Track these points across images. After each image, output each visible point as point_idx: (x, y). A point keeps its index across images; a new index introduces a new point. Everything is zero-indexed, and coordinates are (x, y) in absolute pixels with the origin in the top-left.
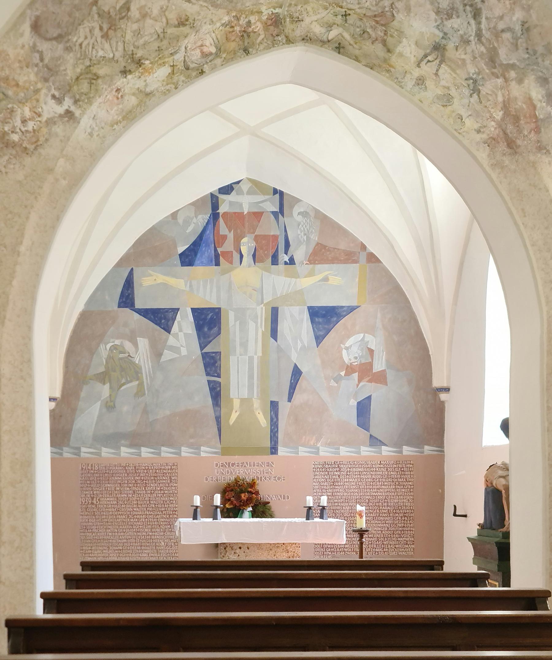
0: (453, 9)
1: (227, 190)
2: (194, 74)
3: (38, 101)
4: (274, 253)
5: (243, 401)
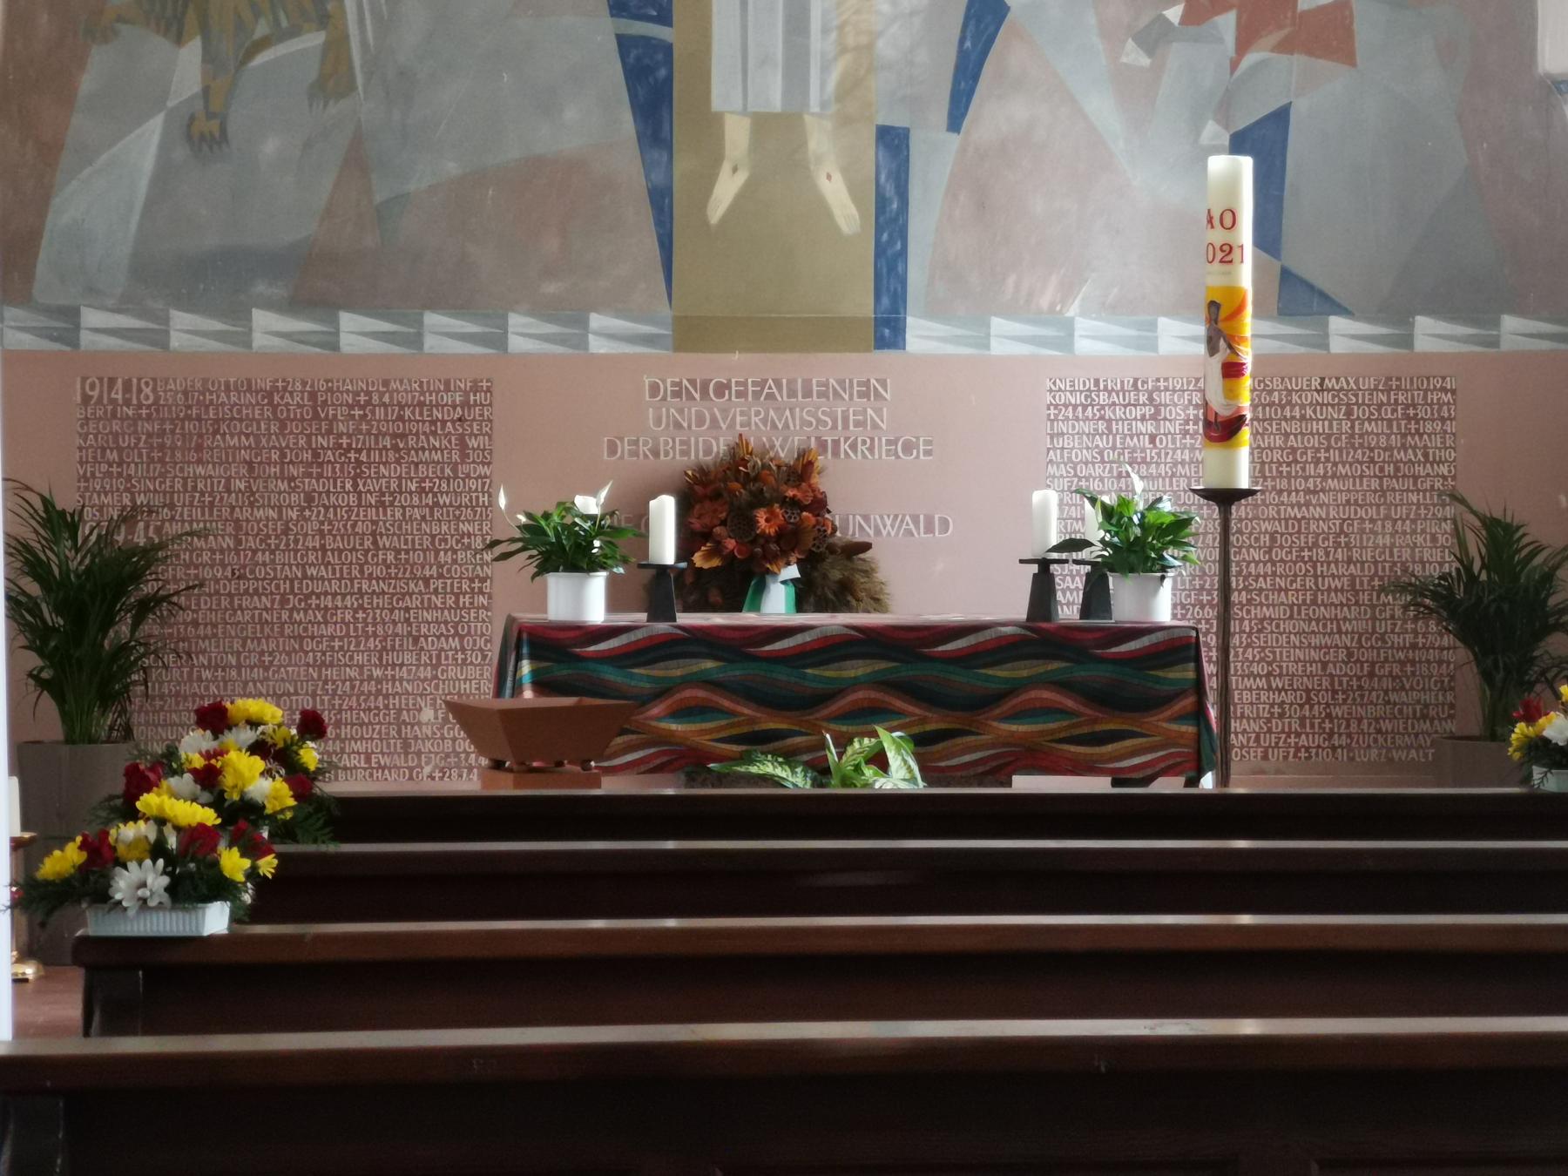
5: (763, 124)
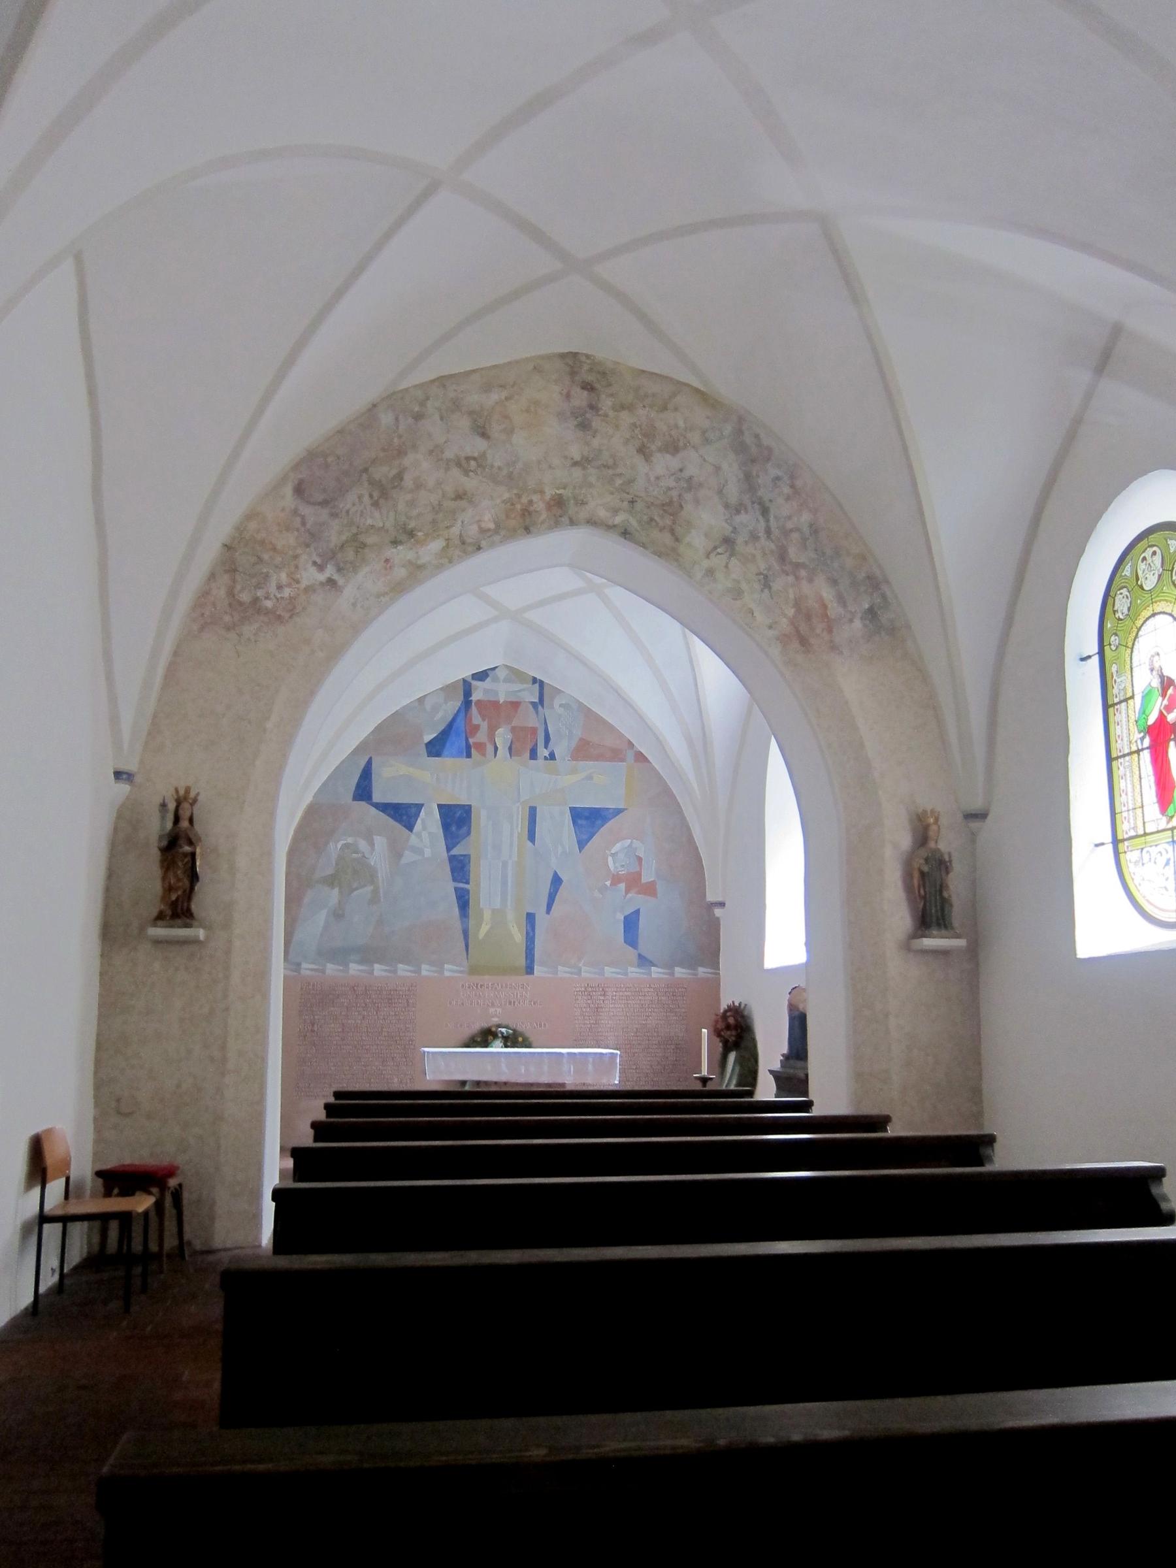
0: (741, 504)
1: (481, 676)
2: (470, 549)
3: (297, 567)
4: (532, 745)
5: (494, 911)
